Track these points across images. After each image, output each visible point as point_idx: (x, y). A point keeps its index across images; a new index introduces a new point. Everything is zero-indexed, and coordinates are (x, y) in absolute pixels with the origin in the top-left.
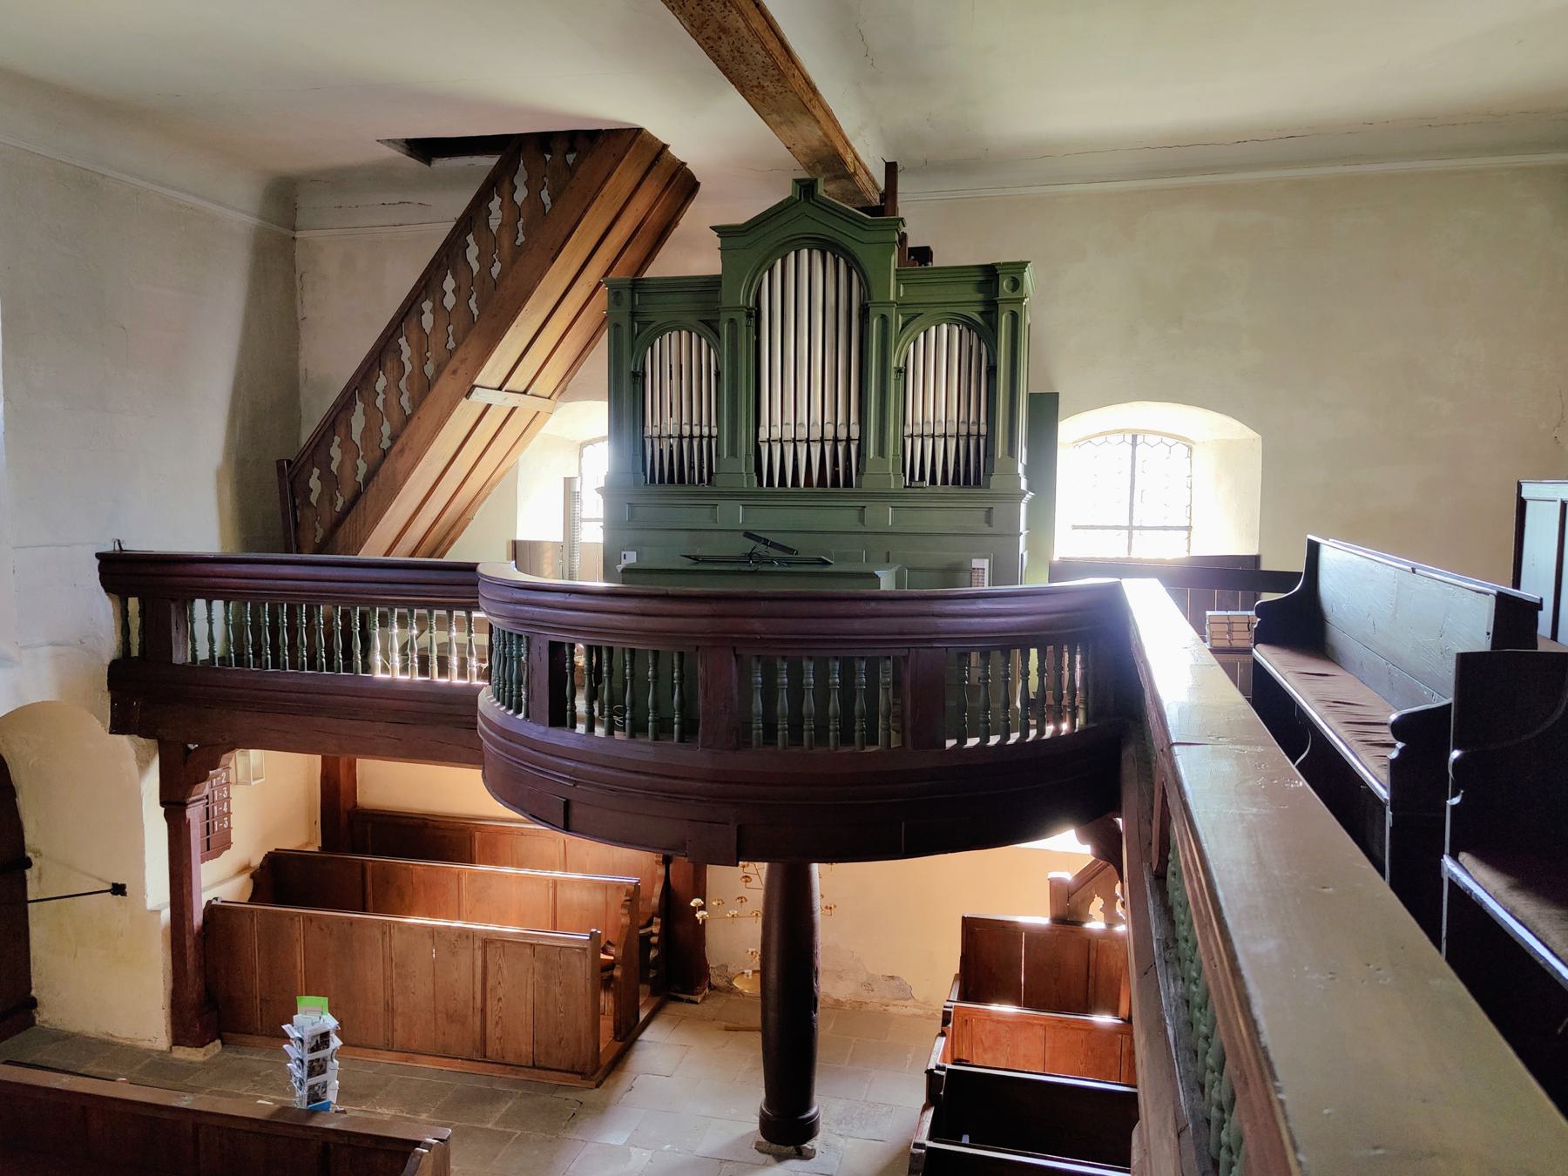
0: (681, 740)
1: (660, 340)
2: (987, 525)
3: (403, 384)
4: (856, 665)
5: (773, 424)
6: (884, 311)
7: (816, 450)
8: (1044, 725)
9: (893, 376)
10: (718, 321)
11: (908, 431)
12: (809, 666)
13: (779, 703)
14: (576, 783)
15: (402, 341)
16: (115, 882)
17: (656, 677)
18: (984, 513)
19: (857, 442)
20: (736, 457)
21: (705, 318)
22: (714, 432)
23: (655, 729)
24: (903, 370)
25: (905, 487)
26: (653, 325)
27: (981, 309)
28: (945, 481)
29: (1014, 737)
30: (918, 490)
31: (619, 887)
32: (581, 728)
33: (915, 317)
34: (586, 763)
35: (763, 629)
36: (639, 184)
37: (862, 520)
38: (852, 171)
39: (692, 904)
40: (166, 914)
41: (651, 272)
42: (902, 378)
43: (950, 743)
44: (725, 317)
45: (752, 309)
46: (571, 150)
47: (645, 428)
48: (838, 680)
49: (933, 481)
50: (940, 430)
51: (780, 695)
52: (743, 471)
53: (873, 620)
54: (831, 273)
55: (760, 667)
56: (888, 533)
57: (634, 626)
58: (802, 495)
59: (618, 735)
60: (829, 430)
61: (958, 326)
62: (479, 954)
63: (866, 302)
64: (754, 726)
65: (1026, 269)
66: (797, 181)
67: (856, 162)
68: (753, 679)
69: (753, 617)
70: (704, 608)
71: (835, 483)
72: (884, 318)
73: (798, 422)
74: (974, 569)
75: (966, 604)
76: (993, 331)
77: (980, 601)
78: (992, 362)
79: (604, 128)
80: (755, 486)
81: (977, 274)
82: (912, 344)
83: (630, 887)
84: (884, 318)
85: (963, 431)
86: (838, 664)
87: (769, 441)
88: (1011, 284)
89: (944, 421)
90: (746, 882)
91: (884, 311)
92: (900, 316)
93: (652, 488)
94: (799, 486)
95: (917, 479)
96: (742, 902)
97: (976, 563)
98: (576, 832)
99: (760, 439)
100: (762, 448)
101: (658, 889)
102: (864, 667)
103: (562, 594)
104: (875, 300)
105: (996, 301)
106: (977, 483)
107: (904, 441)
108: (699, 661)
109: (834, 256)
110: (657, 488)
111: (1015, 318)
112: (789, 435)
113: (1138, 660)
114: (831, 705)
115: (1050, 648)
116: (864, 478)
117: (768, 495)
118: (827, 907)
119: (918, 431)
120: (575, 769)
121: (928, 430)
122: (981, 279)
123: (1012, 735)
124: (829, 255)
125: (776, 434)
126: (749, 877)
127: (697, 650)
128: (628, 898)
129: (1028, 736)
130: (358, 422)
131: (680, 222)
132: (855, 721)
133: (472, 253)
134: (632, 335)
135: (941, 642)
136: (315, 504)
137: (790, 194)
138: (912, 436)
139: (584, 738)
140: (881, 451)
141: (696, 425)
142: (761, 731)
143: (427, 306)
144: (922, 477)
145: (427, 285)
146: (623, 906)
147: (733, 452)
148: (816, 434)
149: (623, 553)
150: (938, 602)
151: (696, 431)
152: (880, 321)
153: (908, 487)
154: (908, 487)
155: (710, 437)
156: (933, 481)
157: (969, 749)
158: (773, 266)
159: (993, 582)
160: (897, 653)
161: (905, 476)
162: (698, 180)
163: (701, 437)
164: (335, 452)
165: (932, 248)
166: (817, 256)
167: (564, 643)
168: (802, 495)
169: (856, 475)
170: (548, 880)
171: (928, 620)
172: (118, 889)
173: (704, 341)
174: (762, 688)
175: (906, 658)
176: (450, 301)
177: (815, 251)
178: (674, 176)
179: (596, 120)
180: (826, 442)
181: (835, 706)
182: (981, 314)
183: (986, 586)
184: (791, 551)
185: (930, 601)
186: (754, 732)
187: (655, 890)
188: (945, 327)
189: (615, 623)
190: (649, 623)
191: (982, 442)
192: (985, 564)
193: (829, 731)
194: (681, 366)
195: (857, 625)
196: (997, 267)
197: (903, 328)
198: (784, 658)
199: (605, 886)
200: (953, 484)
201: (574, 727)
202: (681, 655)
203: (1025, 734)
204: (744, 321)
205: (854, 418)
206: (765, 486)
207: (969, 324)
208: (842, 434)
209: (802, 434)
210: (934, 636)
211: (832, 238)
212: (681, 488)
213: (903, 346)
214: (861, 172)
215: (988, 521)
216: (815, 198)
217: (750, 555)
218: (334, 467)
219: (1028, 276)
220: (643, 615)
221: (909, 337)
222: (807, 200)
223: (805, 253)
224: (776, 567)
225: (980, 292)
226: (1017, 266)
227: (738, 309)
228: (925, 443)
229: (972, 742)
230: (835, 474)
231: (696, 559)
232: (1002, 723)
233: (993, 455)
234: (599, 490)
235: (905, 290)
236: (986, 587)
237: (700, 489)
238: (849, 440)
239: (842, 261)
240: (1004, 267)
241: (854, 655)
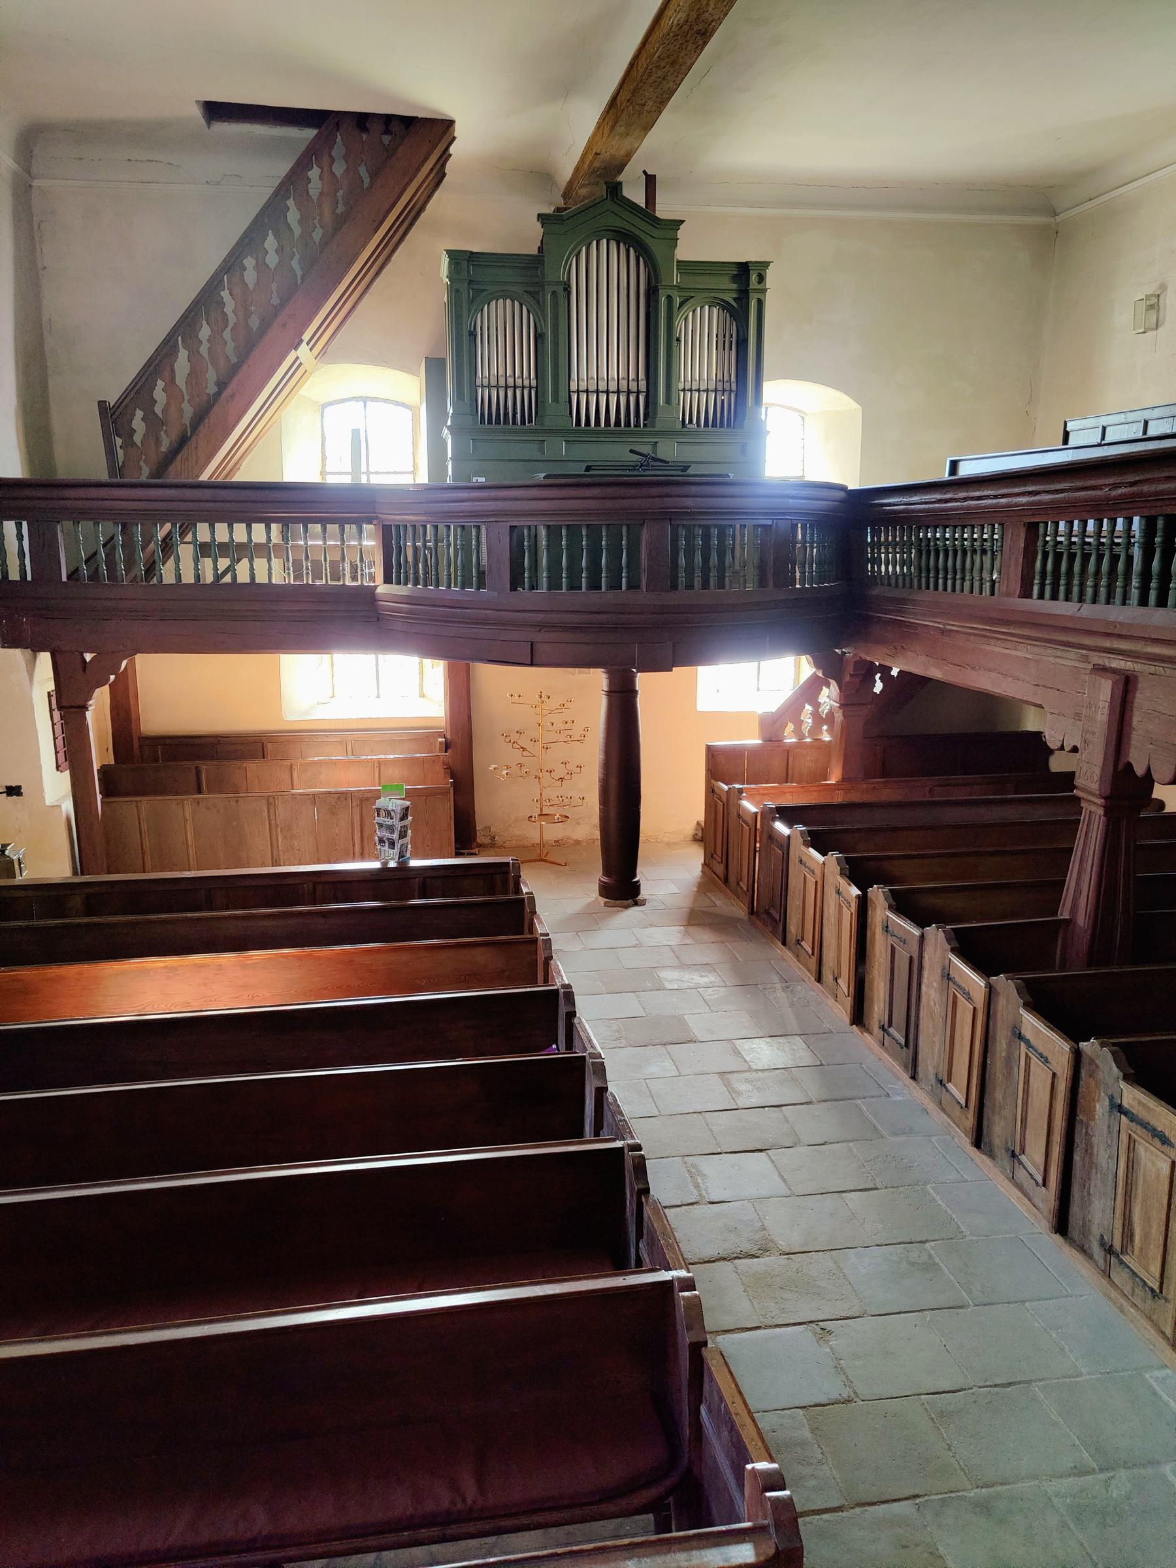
3: (227, 334)
6: (670, 292)
15: (225, 294)
16: (9, 785)
27: (735, 296)
40: (68, 806)
44: (549, 290)
46: (387, 132)
50: (602, 386)
58: (612, 432)
60: (623, 383)
62: (357, 811)
71: (628, 424)
72: (669, 298)
78: (741, 337)
79: (420, 115)
81: (733, 269)
84: (669, 298)
88: (757, 280)
89: (595, 377)
91: (670, 292)
100: (572, 397)
104: (663, 284)
106: (729, 425)
111: (760, 303)
112: (593, 387)
113: (447, 676)
118: (578, 767)
119: (688, 387)
122: (735, 273)
124: (621, 244)
125: (583, 386)
130: (182, 364)
133: (293, 216)
136: (140, 445)
141: (623, 378)
143: (249, 262)
144: (691, 421)
145: (249, 241)
148: (494, 382)
161: (572, 417)
164: (159, 394)
166: (613, 245)
168: (612, 432)
170: (374, 762)
172: (13, 791)
173: (524, 307)
176: (272, 259)
177: (611, 242)
179: (435, 112)
182: (735, 299)
188: (707, 307)
205: (641, 375)
207: (725, 306)
218: (158, 409)
219: (770, 274)
228: (590, 397)
238: (638, 392)
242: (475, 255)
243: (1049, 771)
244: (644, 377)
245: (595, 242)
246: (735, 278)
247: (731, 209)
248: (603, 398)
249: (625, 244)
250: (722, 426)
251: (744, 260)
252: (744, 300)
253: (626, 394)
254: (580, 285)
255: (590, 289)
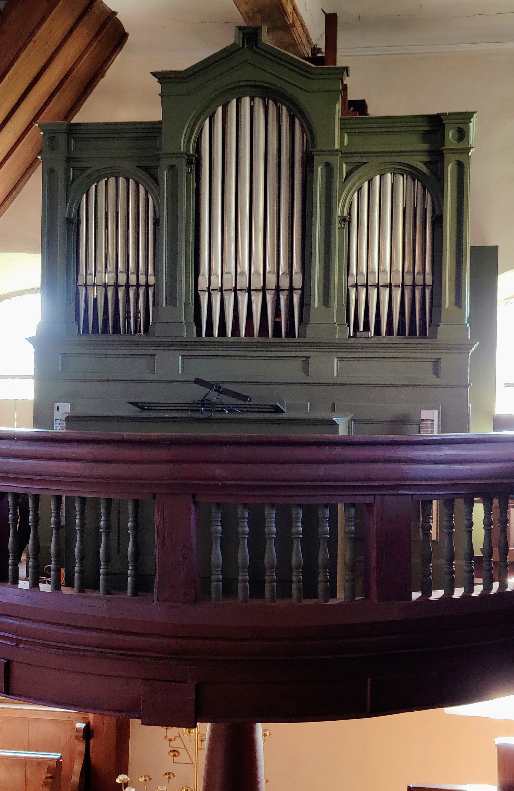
0: (135, 593)
1: (96, 187)
2: (434, 376)
4: (320, 512)
5: (213, 272)
6: (329, 159)
7: (257, 300)
8: (474, 586)
9: (338, 225)
10: (157, 167)
11: (352, 280)
12: (271, 514)
13: (240, 551)
14: (18, 642)
17: (108, 527)
18: (432, 363)
19: (300, 291)
20: (176, 306)
21: (142, 164)
22: (152, 280)
23: (106, 581)
24: (347, 219)
25: (350, 337)
26: (89, 172)
27: (426, 158)
28: (390, 331)
29: (458, 593)
30: (362, 340)
31: (40, 763)
32: (24, 585)
33: (358, 167)
34: (30, 620)
35: (225, 475)
36: (71, 31)
37: (306, 371)
38: (291, 21)
39: (118, 781)
41: (77, 119)
42: (346, 227)
43: (416, 595)
45: (192, 155)
47: (79, 277)
48: (301, 529)
49: (378, 331)
50: (385, 280)
51: (241, 543)
52: (183, 320)
53: (337, 466)
54: (273, 121)
55: (220, 515)
56: (332, 384)
57: (87, 473)
59: (65, 590)
61: (403, 175)
63: (310, 150)
64: (213, 577)
65: (472, 120)
66: (240, 28)
67: (294, 13)
68: (213, 528)
69: (214, 462)
70: (163, 453)
71: (277, 332)
72: (328, 167)
73: (239, 271)
74: (423, 420)
75: (431, 450)
76: (439, 180)
77: (445, 447)
78: (437, 213)
80: (195, 335)
81: (423, 124)
82: (356, 194)
83: (52, 763)
84: (328, 167)
85: (408, 281)
86: (301, 512)
87: (209, 290)
88: (457, 136)
89: (261, 272)
90: (174, 756)
91: (329, 159)
92: (344, 165)
93: (85, 337)
94: (239, 335)
95: (361, 329)
96: (170, 778)
97: (425, 415)
98: (19, 696)
99: (199, 288)
100: (202, 297)
101: (78, 767)
102: (327, 515)
103: (7, 441)
104: (319, 149)
105: (442, 151)
106: (423, 333)
107: (348, 290)
108: (156, 509)
109: (276, 105)
110: (91, 337)
114: (294, 554)
115: (496, 502)
116: (309, 328)
117: (205, 344)
119: (363, 280)
120: (18, 627)
121: (373, 280)
122: (426, 129)
123: (456, 590)
125: (216, 283)
126: (177, 751)
127: (154, 498)
128: (49, 775)
129: (491, 589)
131: (107, 72)
132: (319, 572)
134: (67, 181)
135: (406, 490)
137: (233, 42)
138: (356, 286)
139: (29, 594)
140: (326, 300)
142: (221, 583)
144: (367, 327)
146: (45, 784)
147: (172, 300)
148: (257, 283)
149: (56, 405)
150: (405, 447)
151: (133, 279)
152: (325, 170)
153: (352, 337)
154: (352, 337)
155: (147, 286)
156: (378, 331)
157: (435, 602)
158: (214, 114)
159: (442, 429)
160: (360, 500)
161: (349, 326)
162: (126, 30)
163: (138, 285)
165: (367, 102)
167: (7, 493)
169: (299, 325)
171: (394, 466)
174: (221, 538)
175: (370, 506)
178: (103, 26)
180: (267, 292)
181: (298, 557)
182: (426, 163)
183: (436, 433)
184: (245, 398)
185: (395, 447)
186: (214, 584)
187: (75, 767)
188: (389, 176)
189: (69, 471)
190: (102, 470)
191: (428, 292)
192: (434, 415)
193: (291, 582)
194: (117, 213)
195: (322, 470)
196: (442, 117)
197: (347, 177)
198: (245, 506)
199: (25, 762)
200: (398, 334)
201: (15, 581)
202: (136, 503)
203: (470, 588)
204: (185, 167)
205: (296, 267)
206: (204, 335)
208: (285, 283)
209: (243, 283)
210: (399, 483)
211: (271, 84)
212: (116, 338)
213: (347, 197)
214: (298, 24)
215: (436, 370)
216: (259, 45)
217: (202, 403)
219: (473, 126)
220: (96, 461)
221: (353, 186)
222: (250, 48)
223: (246, 101)
224: (227, 414)
225: (424, 141)
226: (463, 116)
227: (178, 155)
228: (370, 292)
229: (437, 594)
230: (277, 325)
231: (141, 407)
232: (446, 577)
233: (440, 306)
234: (30, 340)
235: (349, 139)
236: (435, 434)
237: (136, 338)
238: (291, 289)
239: (284, 110)
240: (449, 117)
241: (319, 502)
242: (75, 127)
243: (116, 780)
244: (299, 270)
245: (234, 101)
246: (426, 136)
247: (493, 46)
248: (243, 299)
249: (275, 102)
250: (412, 333)
251: (434, 111)
252: (439, 163)
253: (273, 292)
254: (215, 153)
255: (227, 159)
